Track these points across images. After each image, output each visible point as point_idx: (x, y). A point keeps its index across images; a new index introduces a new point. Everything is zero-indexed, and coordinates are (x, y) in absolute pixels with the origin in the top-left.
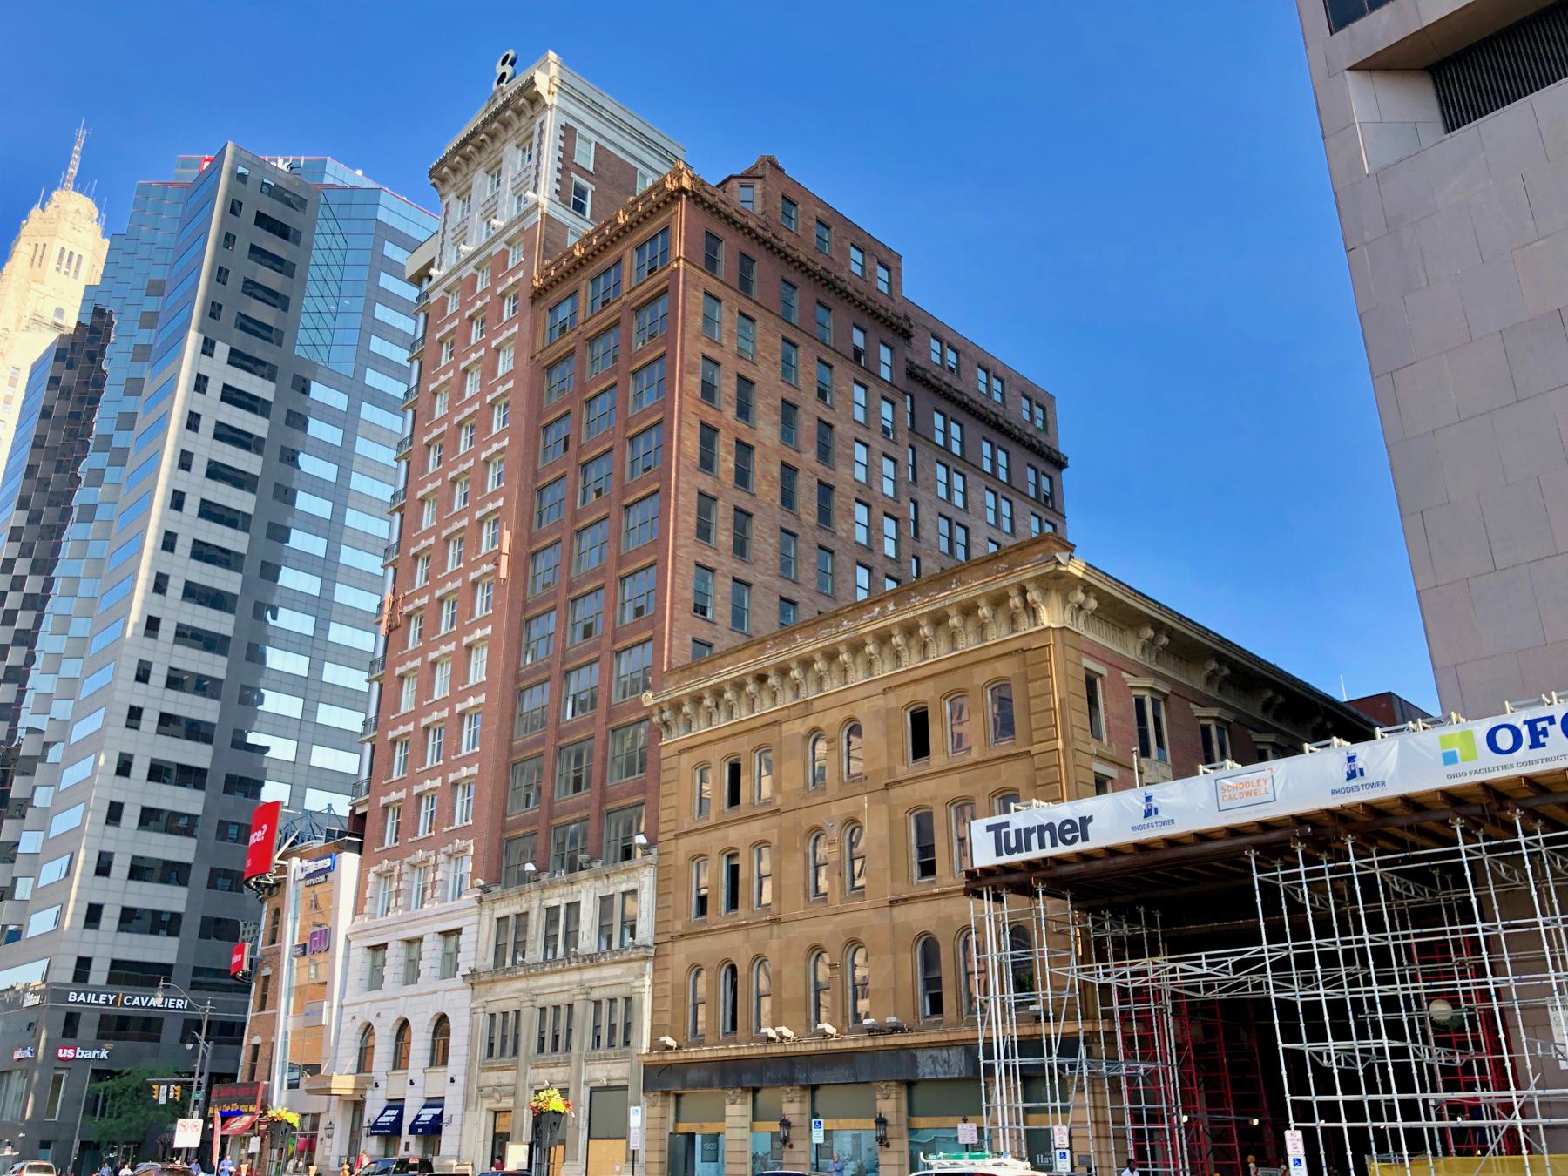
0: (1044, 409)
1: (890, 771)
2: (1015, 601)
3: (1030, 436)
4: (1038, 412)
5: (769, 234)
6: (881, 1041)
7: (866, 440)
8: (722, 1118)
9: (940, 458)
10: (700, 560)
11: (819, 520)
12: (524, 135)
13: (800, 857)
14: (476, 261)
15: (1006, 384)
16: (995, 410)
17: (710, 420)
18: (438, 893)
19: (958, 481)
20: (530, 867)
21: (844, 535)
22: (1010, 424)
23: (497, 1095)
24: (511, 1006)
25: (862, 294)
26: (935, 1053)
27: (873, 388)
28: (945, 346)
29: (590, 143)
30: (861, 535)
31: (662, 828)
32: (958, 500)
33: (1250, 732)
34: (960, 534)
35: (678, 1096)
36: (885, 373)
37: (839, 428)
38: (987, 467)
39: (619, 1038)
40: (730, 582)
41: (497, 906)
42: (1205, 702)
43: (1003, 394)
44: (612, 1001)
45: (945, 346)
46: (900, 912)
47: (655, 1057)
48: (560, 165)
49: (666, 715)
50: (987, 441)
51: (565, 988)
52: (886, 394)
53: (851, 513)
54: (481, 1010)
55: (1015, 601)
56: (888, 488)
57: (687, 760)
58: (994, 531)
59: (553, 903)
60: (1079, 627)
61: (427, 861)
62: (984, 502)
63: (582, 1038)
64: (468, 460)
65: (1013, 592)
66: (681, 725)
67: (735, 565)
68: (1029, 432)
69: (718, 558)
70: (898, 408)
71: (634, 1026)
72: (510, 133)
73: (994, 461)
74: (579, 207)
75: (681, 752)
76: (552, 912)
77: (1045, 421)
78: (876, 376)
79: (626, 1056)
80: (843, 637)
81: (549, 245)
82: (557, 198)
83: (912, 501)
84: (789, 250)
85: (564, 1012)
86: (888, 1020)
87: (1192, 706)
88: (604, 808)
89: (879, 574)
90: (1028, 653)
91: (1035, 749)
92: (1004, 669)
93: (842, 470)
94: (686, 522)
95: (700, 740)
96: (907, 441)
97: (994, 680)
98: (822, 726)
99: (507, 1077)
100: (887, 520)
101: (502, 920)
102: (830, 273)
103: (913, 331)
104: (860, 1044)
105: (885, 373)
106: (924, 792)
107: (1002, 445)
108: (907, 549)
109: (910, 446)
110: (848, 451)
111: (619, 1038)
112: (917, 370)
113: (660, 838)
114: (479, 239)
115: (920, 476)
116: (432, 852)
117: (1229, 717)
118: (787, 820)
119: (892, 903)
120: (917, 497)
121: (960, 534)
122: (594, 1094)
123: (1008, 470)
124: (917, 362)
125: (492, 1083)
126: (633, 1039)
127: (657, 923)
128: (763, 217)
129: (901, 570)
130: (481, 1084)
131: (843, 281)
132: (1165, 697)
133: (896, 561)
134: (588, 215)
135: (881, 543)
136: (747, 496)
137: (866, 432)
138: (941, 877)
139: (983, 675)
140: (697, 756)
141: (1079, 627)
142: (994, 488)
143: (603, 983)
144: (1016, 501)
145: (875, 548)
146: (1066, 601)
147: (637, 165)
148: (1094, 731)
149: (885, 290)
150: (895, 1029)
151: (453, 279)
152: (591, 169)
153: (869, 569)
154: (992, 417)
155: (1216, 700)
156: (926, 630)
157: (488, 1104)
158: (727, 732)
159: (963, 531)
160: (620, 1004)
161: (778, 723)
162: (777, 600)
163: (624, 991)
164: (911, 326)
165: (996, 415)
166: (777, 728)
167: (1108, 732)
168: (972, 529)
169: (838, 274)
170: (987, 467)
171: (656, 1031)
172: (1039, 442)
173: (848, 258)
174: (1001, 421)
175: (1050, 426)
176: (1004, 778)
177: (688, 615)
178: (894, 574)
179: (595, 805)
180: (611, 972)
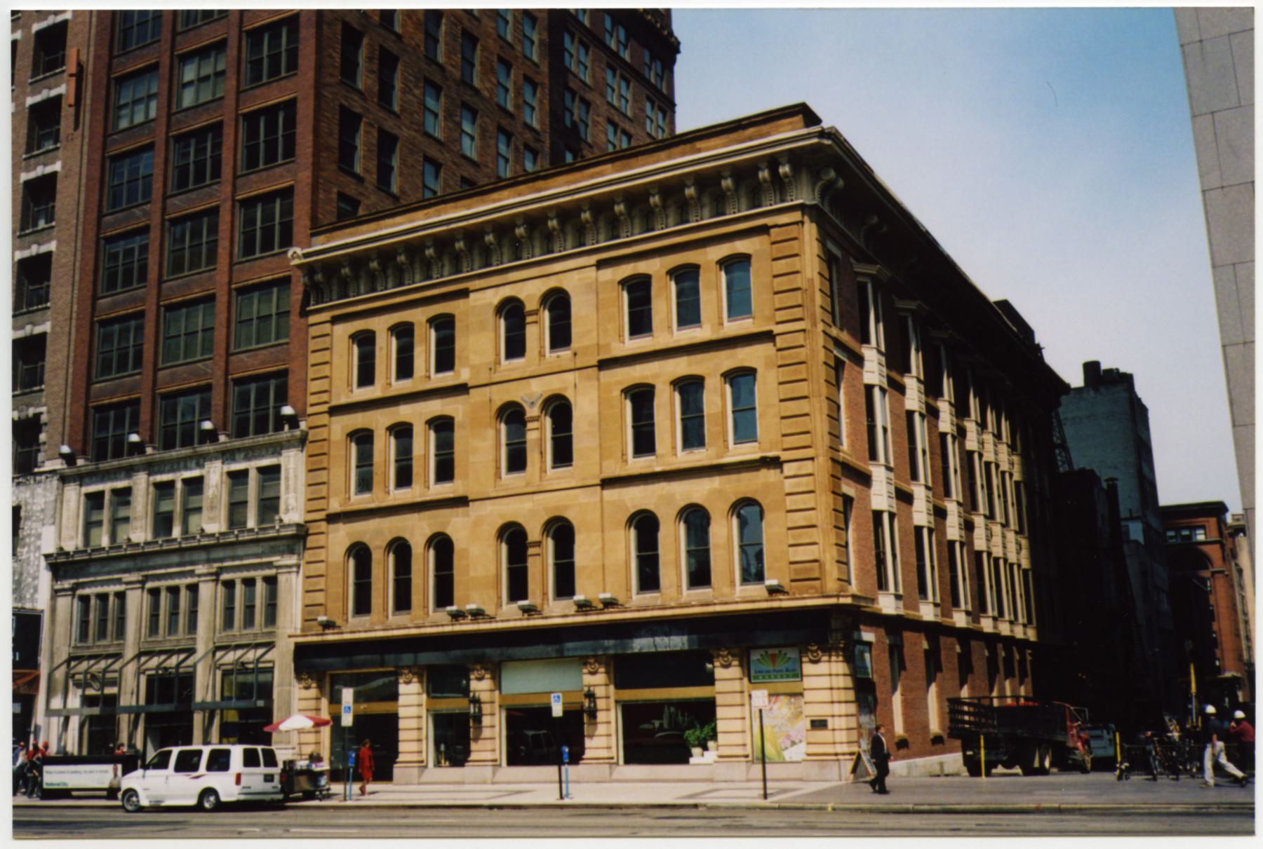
2: (764, 174)
49: (319, 277)
55: (764, 174)
66: (335, 288)
85: (184, 596)
88: (230, 377)
92: (741, 246)
98: (522, 296)
113: (310, 410)
138: (663, 456)
177: (334, 167)
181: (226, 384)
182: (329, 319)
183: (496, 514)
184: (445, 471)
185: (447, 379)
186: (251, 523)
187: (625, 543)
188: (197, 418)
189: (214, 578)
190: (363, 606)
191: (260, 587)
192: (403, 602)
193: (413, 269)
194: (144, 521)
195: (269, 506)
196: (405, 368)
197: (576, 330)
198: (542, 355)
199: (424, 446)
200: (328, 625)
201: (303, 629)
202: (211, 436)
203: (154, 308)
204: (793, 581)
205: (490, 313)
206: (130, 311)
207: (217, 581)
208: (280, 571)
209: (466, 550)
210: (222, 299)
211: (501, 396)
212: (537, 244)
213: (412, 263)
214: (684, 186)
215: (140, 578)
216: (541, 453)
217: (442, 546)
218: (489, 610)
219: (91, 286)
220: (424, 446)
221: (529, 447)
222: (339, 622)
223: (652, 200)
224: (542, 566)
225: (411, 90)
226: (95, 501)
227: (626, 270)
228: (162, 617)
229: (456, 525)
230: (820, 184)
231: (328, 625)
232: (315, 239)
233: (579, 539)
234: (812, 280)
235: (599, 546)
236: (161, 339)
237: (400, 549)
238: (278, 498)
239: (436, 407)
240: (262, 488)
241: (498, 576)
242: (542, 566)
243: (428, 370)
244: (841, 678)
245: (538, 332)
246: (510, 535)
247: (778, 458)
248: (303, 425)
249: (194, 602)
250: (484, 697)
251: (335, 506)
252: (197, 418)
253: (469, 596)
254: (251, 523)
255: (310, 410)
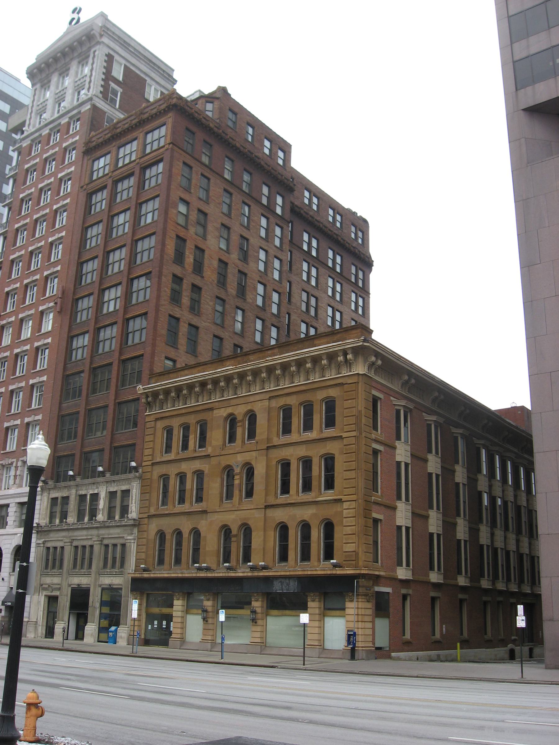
0: (363, 233)
1: (269, 440)
3: (354, 248)
4: (360, 234)
5: (221, 131)
6: (256, 574)
7: (266, 248)
8: (171, 606)
9: (305, 258)
10: (171, 313)
11: (238, 292)
12: (84, 57)
13: (219, 480)
14: (51, 126)
15: (344, 218)
16: (336, 232)
17: (181, 235)
18: (17, 481)
19: (314, 272)
20: (71, 473)
21: (251, 301)
22: (344, 240)
23: (50, 589)
24: (59, 544)
25: (269, 166)
26: (283, 580)
27: (272, 219)
28: (312, 195)
29: (121, 65)
30: (260, 301)
31: (145, 458)
32: (313, 283)
33: (451, 427)
34: (313, 301)
35: (148, 595)
36: (279, 211)
37: (252, 240)
38: (330, 264)
39: (118, 564)
40: (187, 326)
41: (51, 492)
42: (431, 412)
43: (341, 224)
44: (115, 545)
45: (312, 195)
46: (270, 513)
47: (137, 575)
48: (103, 77)
49: (150, 399)
50: (331, 249)
51: (89, 537)
52: (279, 222)
53: (255, 289)
54: (42, 545)
55: (341, 358)
56: (276, 276)
57: (160, 425)
58: (331, 300)
59: (83, 492)
60: (372, 374)
61: (12, 463)
62: (327, 283)
63: (97, 563)
64: (26, 219)
65: (341, 354)
67: (190, 317)
68: (354, 245)
69: (181, 312)
70: (284, 231)
71: (127, 559)
72: (76, 54)
73: (334, 261)
74: (113, 101)
75: (157, 419)
76: (82, 498)
77: (363, 240)
78: (274, 213)
79: (121, 574)
80: (250, 367)
81: (95, 123)
82: (101, 96)
83: (289, 281)
84: (231, 140)
85: (88, 550)
86: (260, 564)
87: (424, 414)
88: (113, 445)
89: (268, 323)
90: (345, 385)
91: (344, 435)
92: (332, 392)
93: (252, 264)
94: (165, 291)
95: (167, 414)
96: (288, 248)
97: (327, 398)
98: (236, 413)
99: (56, 580)
100: (274, 293)
101: (54, 500)
102: (252, 153)
103: (295, 188)
104: (245, 574)
105: (279, 211)
106: (286, 453)
107: (339, 252)
108: (284, 310)
109: (290, 251)
110: (256, 254)
111: (118, 564)
112: (296, 208)
114: (53, 113)
115: (294, 268)
116: (15, 460)
117: (441, 420)
118: (214, 461)
119: (267, 507)
120: (291, 279)
121: (313, 301)
122: (103, 591)
123: (341, 266)
124: (296, 203)
125: (48, 582)
126: (126, 565)
127: (140, 508)
128: (218, 121)
129: (280, 321)
130: (42, 583)
131: (259, 158)
132: (411, 410)
133: (278, 316)
134: (117, 106)
135: (270, 306)
136: (199, 278)
137: (266, 244)
139: (321, 395)
140: (166, 423)
141: (372, 374)
142: (333, 276)
143: (110, 536)
144: (344, 284)
145: (267, 308)
146: (365, 360)
147: (147, 78)
148: (375, 428)
149: (282, 164)
150: (264, 568)
151: (37, 134)
152: (121, 79)
153: (263, 321)
154: (335, 236)
155: (435, 411)
156: (294, 368)
157: (45, 593)
158: (183, 411)
159: (315, 299)
160: (119, 548)
161: (212, 409)
162: (212, 337)
163: (122, 541)
164: (295, 185)
165: (337, 235)
166: (211, 412)
167: (381, 427)
168: (319, 298)
169: (257, 154)
170: (330, 264)
171: (138, 562)
172: (359, 251)
173: (263, 146)
174: (339, 239)
175: (365, 242)
176: (328, 448)
178: (276, 324)
179: (108, 443)
180: (115, 532)
181: (111, 449)
182: (268, 398)
183: (219, 519)
184: (199, 499)
185: (202, 452)
186: (117, 518)
187: (273, 539)
188: (129, 460)
189: (100, 542)
190: (284, 557)
191: (119, 548)
192: (306, 556)
193: (285, 377)
194: (73, 513)
195: (125, 510)
196: (185, 447)
197: (258, 431)
198: (243, 442)
199: (191, 484)
200: (145, 570)
201: (135, 571)
202: (102, 474)
203: (84, 410)
204: (344, 561)
205: (221, 422)
206: (74, 411)
207: (101, 544)
208: (127, 541)
209: (205, 537)
210: (111, 407)
211: (225, 461)
212: (244, 387)
213: (330, 364)
214: (276, 369)
215: (70, 541)
216: (240, 491)
217: (196, 533)
218: (214, 566)
219: (59, 398)
220: (191, 484)
221: (313, 478)
222: (151, 568)
223: (323, 362)
224: (237, 549)
225: (208, 303)
226: (54, 500)
227: (282, 402)
228: (50, 560)
229: (203, 525)
230: (367, 363)
231: (145, 570)
232: (153, 380)
233: (254, 534)
234: (361, 411)
235: (262, 538)
236: (86, 425)
237: (179, 533)
238: (128, 506)
239: (197, 465)
240: (122, 501)
241: (219, 551)
242: (237, 549)
243: (195, 447)
244: (180, 613)
245: (241, 432)
246: (303, 525)
247: (341, 499)
248: (140, 471)
249: (91, 553)
250: (259, 610)
251: (152, 511)
252: (129, 460)
253: (257, 560)
254: (117, 518)
255: (144, 464)
